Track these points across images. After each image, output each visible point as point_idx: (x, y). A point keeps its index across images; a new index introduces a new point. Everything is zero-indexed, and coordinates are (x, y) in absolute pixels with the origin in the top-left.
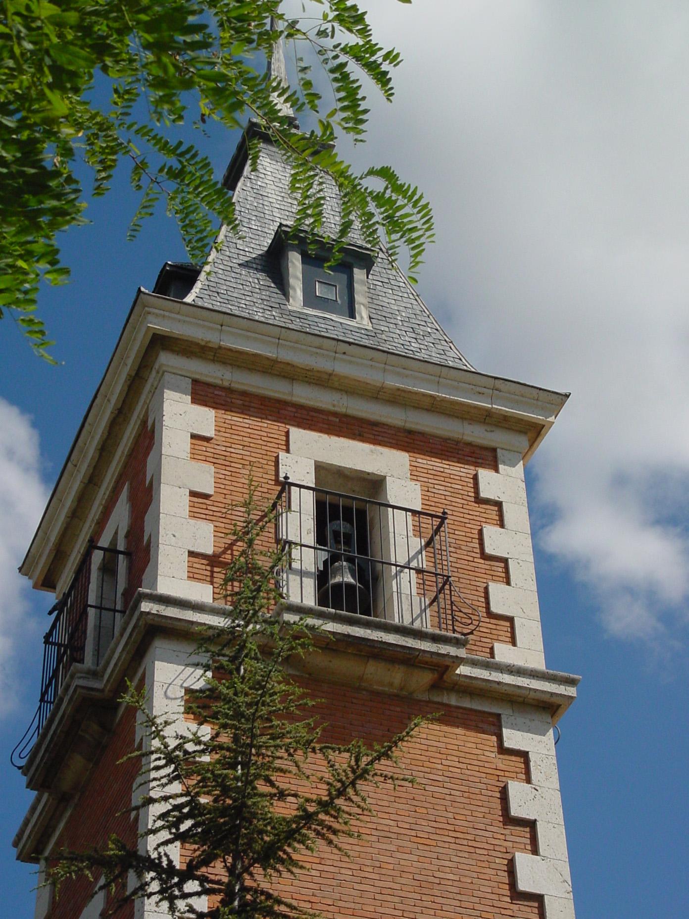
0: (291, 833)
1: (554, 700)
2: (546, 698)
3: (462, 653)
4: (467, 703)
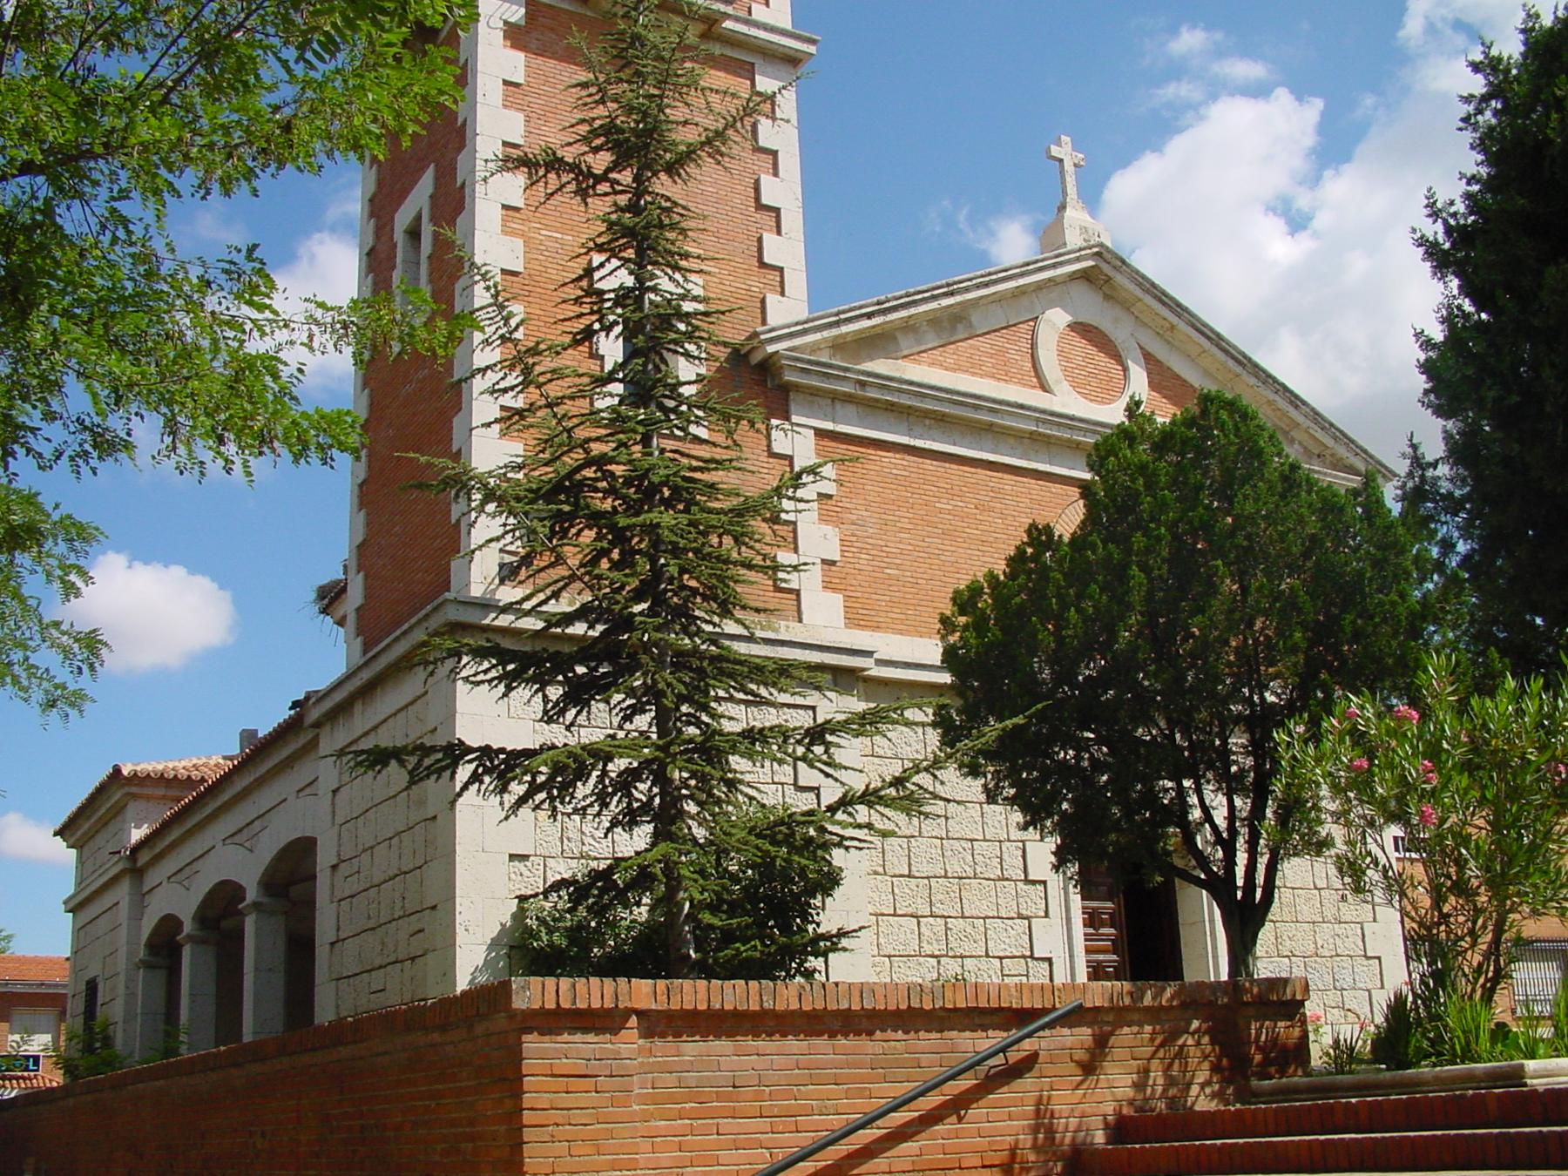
0: (689, 155)
1: (799, 55)
2: (792, 53)
3: (729, 10)
4: (729, 52)
